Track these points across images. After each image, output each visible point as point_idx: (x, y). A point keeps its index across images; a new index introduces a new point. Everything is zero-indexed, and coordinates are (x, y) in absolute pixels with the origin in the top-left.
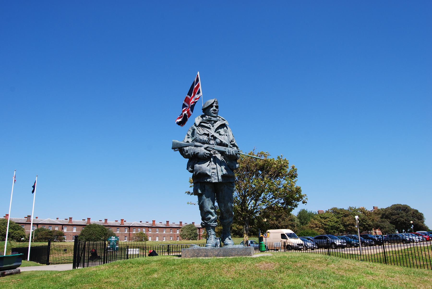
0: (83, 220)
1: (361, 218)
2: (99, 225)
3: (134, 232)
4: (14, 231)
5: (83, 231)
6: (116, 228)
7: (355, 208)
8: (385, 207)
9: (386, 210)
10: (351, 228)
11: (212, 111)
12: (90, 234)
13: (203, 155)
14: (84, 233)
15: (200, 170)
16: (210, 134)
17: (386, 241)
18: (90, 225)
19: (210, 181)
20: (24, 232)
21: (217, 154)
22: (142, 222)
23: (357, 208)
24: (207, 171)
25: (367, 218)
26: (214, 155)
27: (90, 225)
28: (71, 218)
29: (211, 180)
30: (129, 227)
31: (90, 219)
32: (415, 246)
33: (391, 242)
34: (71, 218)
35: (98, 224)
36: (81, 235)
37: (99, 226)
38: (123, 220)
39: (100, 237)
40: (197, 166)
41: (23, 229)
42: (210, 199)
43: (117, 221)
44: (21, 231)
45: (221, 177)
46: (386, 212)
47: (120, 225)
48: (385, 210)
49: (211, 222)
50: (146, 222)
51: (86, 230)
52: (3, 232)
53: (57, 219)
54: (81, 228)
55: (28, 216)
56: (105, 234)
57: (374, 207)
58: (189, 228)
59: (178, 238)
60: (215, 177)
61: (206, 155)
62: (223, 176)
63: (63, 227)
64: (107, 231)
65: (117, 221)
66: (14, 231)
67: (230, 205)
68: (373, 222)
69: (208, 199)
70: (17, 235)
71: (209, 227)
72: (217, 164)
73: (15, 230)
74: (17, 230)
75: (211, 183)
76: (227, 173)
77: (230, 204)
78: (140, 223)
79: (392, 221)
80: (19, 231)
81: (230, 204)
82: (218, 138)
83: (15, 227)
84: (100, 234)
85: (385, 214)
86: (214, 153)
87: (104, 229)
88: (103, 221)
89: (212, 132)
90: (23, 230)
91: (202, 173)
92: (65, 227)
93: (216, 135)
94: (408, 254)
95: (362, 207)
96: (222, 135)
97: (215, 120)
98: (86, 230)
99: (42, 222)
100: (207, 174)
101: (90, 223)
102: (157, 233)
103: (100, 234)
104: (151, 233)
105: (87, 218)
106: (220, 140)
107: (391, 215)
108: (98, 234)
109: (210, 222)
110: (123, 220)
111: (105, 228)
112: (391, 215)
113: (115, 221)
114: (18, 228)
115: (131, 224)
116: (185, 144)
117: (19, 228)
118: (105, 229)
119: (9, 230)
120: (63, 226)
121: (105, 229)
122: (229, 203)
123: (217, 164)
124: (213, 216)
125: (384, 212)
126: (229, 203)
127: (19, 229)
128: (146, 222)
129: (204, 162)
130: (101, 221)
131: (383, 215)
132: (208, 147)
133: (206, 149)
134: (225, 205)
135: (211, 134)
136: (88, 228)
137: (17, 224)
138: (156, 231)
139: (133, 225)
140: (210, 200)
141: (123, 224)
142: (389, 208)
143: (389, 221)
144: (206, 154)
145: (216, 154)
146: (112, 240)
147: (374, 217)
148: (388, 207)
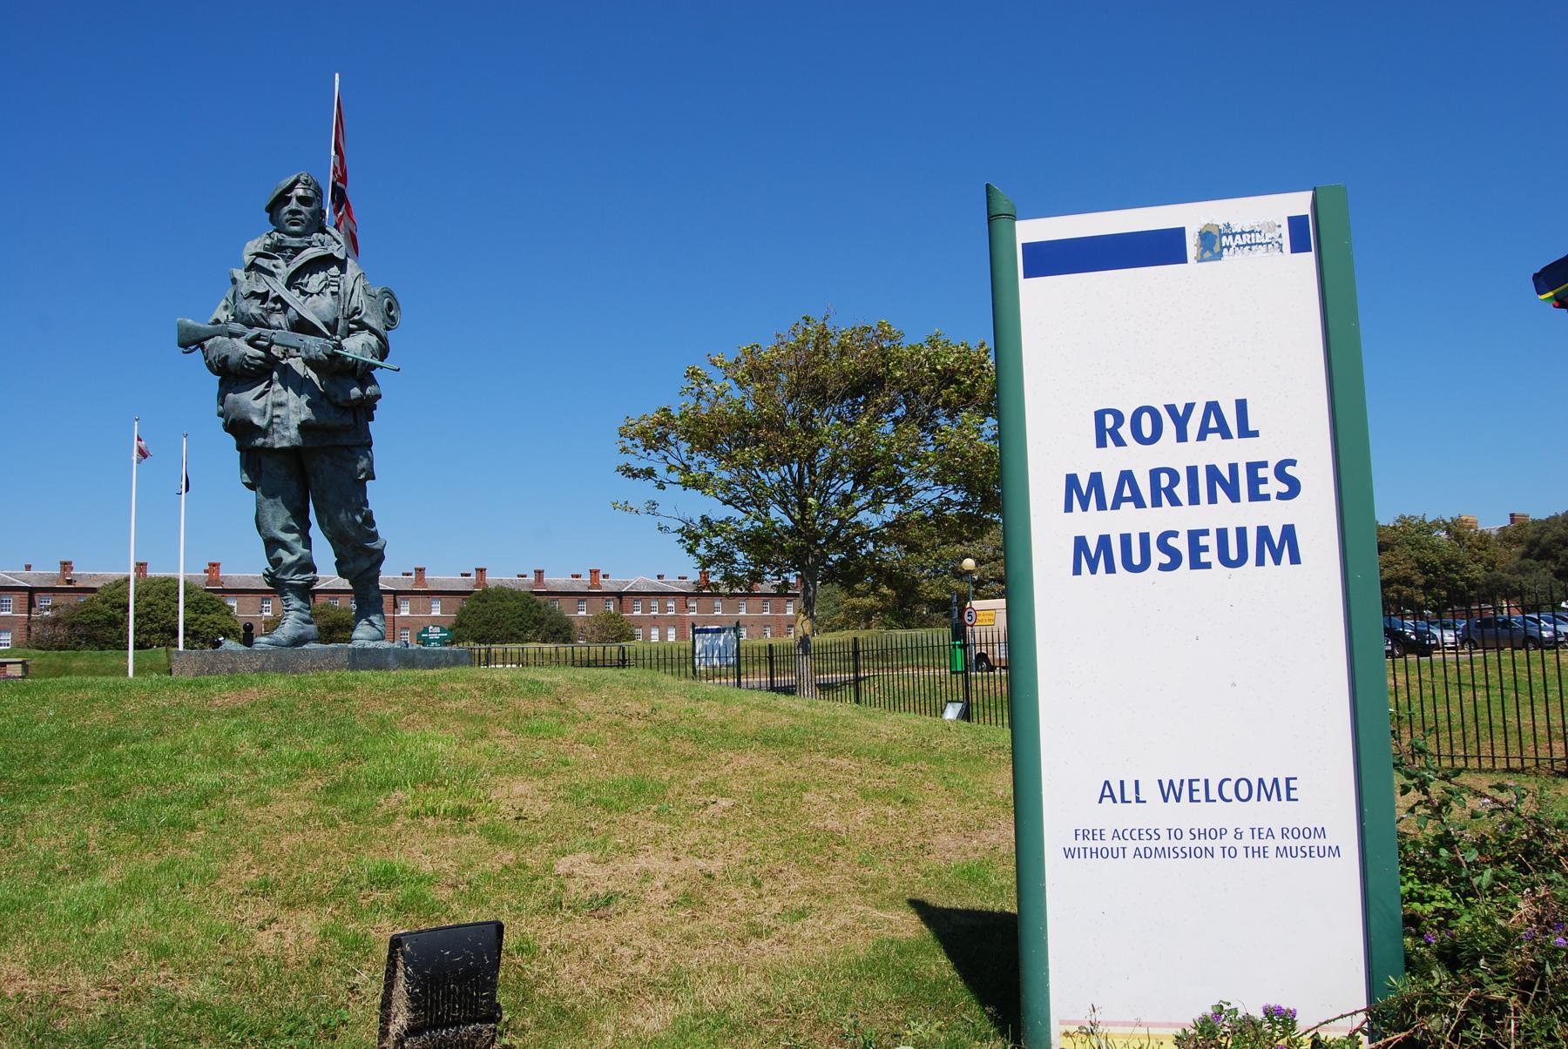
0: (462, 575)
1: (1442, 556)
2: (516, 590)
3: (635, 613)
4: (198, 615)
5: (462, 613)
6: (573, 600)
7: (1423, 519)
8: (1544, 517)
9: (1547, 525)
10: (1399, 592)
11: (288, 216)
12: (487, 623)
13: (238, 363)
14: (465, 621)
15: (233, 411)
16: (271, 291)
17: (1467, 640)
18: (486, 592)
19: (264, 443)
20: (232, 619)
21: (295, 357)
22: (663, 576)
23: (1428, 520)
24: (253, 413)
25: (1463, 555)
26: (284, 362)
27: (486, 591)
28: (420, 570)
29: (269, 440)
30: (619, 595)
31: (485, 570)
32: (1507, 657)
33: (1483, 644)
34: (420, 571)
35: (511, 589)
36: (456, 624)
37: (514, 595)
38: (595, 573)
39: (520, 630)
40: (230, 396)
41: (228, 610)
42: (279, 500)
43: (577, 576)
44: (222, 615)
45: (299, 432)
46: (1543, 534)
47: (589, 588)
48: (1542, 528)
49: (285, 572)
50: (679, 578)
51: (473, 607)
52: (163, 620)
53: (28, 567)
54: (456, 602)
55: (210, 564)
56: (535, 619)
57: (1512, 515)
58: (828, 594)
59: (792, 631)
60: (282, 431)
61: (251, 362)
62: (304, 427)
63: (398, 600)
64: (543, 610)
65: (577, 576)
66: (198, 615)
67: (345, 519)
68: (1492, 571)
69: (271, 500)
70: (209, 627)
71: (282, 587)
72: (289, 388)
73: (203, 613)
74: (208, 614)
75: (271, 451)
76: (313, 418)
77: (347, 515)
78: (656, 580)
79: (1563, 567)
80: (214, 616)
81: (347, 515)
82: (293, 305)
83: (201, 605)
84: (521, 619)
85: (1539, 542)
86: (284, 354)
87: (533, 603)
88: (531, 578)
89: (278, 287)
90: (228, 614)
91: (239, 421)
92: (404, 599)
93: (288, 296)
94: (1476, 689)
95: (1455, 516)
96: (312, 295)
97: (297, 245)
98: (473, 610)
99: (326, 586)
100: (251, 422)
101: (484, 584)
102: (716, 613)
103: (521, 619)
104: (695, 614)
105: (476, 569)
106: (297, 312)
107: (1560, 546)
108: (514, 623)
109: (281, 573)
110: (598, 571)
111: (535, 601)
112: (1560, 546)
113: (573, 576)
114: (212, 605)
115: (626, 586)
116: (208, 330)
117: (215, 606)
118: (534, 605)
119: (185, 613)
120: (398, 598)
121: (534, 605)
122: (343, 510)
123: (289, 388)
124: (292, 554)
125: (1535, 533)
126: (343, 510)
127: (213, 609)
128: (679, 578)
129: (253, 384)
130: (525, 576)
131: (1533, 544)
132: (258, 337)
133: (251, 343)
134: (329, 519)
135: (275, 292)
136: (478, 603)
137: (209, 594)
138: (714, 609)
139: (631, 588)
140: (281, 504)
141: (599, 587)
142: (1556, 517)
143: (1553, 566)
144: (248, 359)
145: (291, 357)
146: (431, 637)
147: (1494, 554)
148: (1553, 514)
